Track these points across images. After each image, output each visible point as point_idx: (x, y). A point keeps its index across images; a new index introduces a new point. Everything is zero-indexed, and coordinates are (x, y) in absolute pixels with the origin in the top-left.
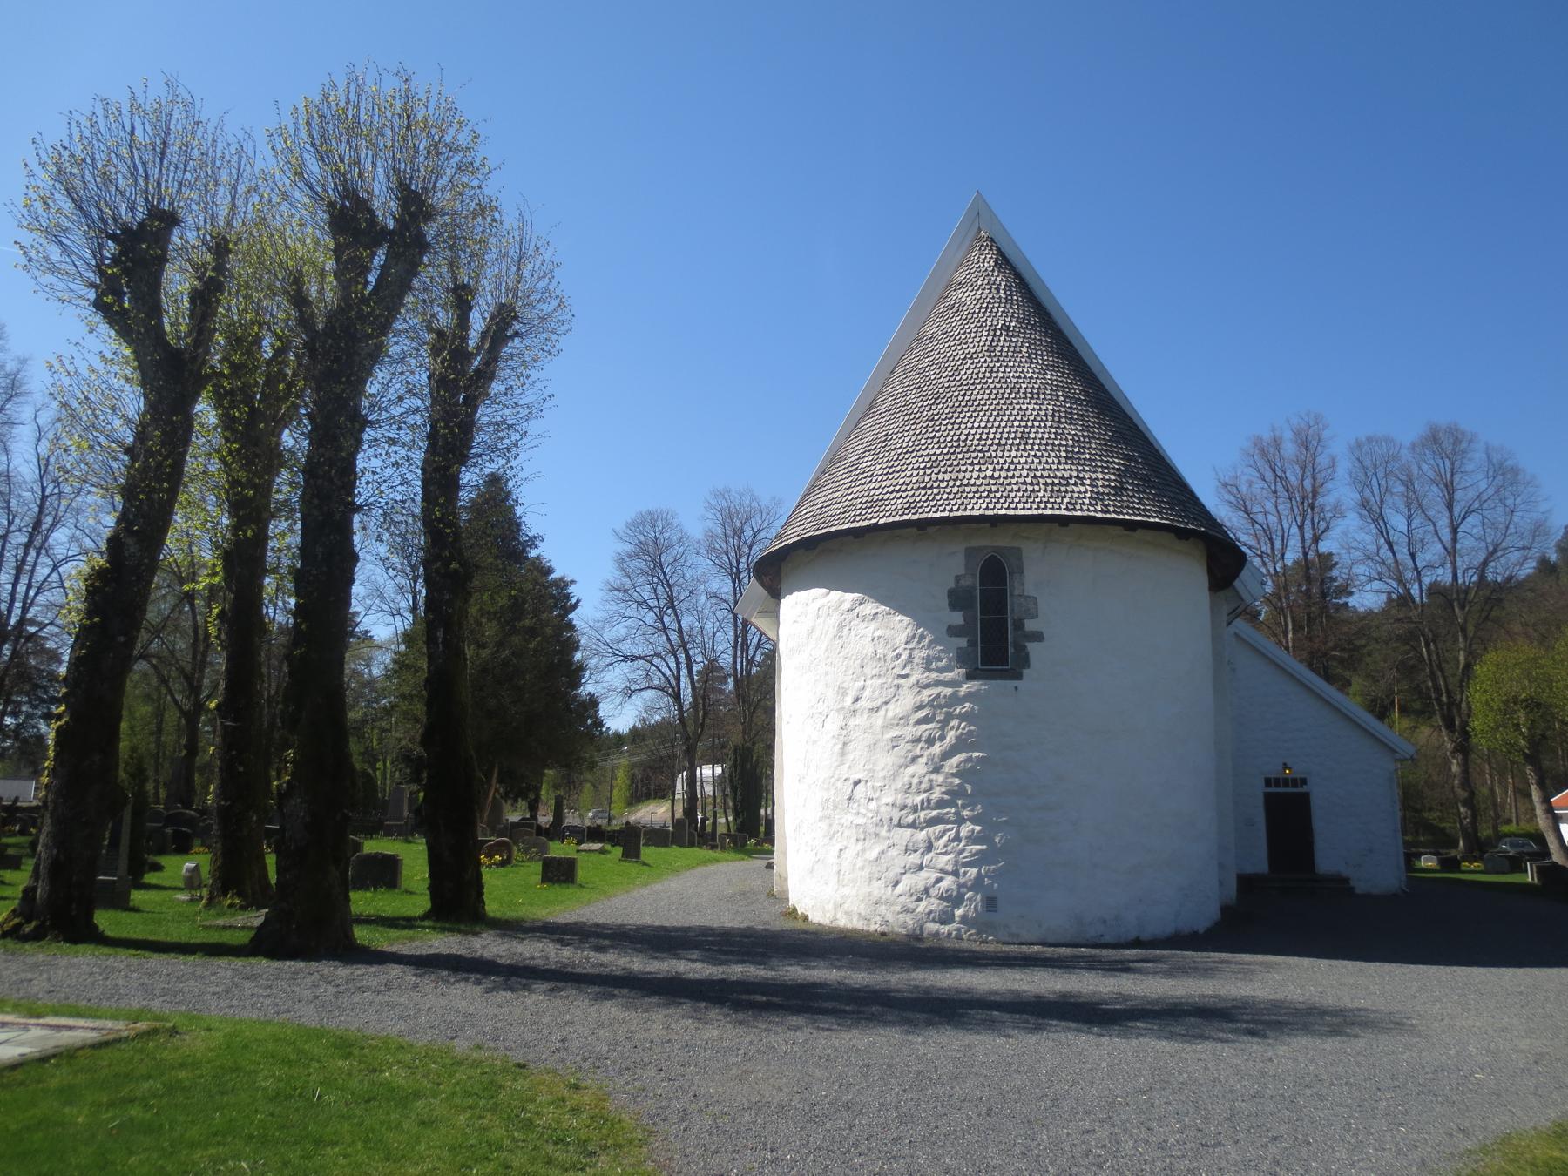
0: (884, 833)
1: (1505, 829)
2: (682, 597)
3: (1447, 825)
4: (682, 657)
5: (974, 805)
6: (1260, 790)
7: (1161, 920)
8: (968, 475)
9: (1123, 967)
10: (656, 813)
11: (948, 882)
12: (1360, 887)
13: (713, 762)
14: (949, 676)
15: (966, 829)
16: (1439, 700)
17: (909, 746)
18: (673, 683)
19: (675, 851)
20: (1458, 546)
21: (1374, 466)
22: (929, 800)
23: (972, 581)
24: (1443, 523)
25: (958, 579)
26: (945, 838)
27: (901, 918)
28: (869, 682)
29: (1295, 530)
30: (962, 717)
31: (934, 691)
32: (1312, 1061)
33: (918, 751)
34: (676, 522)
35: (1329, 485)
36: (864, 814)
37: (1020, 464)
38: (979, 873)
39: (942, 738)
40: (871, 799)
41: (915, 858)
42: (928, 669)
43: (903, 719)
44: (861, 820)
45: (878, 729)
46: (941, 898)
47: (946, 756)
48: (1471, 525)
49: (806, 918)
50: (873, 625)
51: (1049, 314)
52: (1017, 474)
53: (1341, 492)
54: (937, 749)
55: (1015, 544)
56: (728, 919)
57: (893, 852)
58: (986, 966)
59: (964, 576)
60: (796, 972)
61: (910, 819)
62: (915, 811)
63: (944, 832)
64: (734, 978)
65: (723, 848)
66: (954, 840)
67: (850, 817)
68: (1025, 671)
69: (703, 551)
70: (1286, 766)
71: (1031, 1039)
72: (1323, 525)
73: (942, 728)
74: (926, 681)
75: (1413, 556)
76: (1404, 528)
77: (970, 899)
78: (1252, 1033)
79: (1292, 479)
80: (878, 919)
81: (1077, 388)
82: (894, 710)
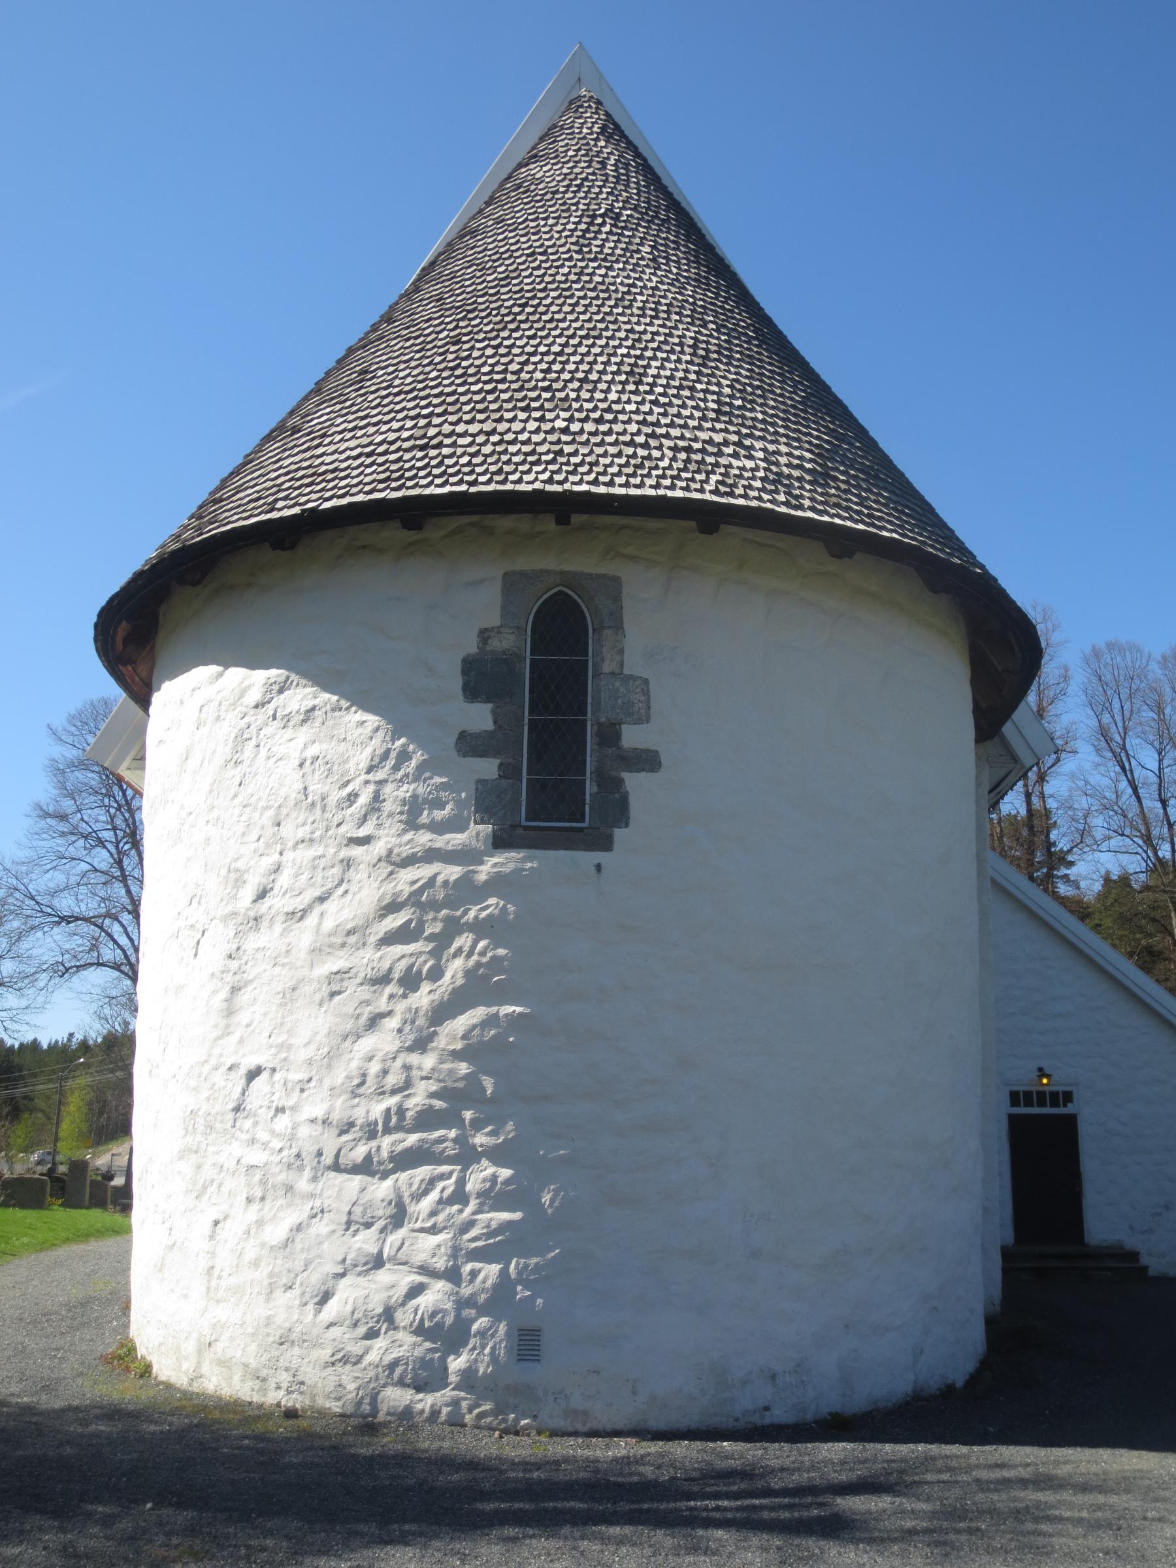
0: (303, 1184)
7: (886, 1378)
11: (436, 1295)
14: (456, 840)
15: (479, 1175)
17: (365, 992)
22: (401, 1111)
23: (515, 642)
25: (484, 635)
26: (434, 1196)
28: (289, 856)
30: (480, 928)
33: (382, 1004)
36: (260, 1145)
39: (436, 974)
40: (280, 1110)
41: (365, 1242)
42: (411, 824)
43: (355, 932)
44: (257, 1157)
45: (301, 953)
47: (442, 1012)
49: (146, 1371)
50: (304, 734)
52: (618, 428)
54: (424, 998)
57: (321, 1227)
59: (498, 630)
61: (361, 1151)
62: (371, 1132)
63: (432, 1182)
67: (237, 1149)
68: (619, 834)
70: (1042, 1073)
73: (436, 953)
74: (406, 851)
76: (1154, 766)
77: (482, 1334)
80: (284, 1378)
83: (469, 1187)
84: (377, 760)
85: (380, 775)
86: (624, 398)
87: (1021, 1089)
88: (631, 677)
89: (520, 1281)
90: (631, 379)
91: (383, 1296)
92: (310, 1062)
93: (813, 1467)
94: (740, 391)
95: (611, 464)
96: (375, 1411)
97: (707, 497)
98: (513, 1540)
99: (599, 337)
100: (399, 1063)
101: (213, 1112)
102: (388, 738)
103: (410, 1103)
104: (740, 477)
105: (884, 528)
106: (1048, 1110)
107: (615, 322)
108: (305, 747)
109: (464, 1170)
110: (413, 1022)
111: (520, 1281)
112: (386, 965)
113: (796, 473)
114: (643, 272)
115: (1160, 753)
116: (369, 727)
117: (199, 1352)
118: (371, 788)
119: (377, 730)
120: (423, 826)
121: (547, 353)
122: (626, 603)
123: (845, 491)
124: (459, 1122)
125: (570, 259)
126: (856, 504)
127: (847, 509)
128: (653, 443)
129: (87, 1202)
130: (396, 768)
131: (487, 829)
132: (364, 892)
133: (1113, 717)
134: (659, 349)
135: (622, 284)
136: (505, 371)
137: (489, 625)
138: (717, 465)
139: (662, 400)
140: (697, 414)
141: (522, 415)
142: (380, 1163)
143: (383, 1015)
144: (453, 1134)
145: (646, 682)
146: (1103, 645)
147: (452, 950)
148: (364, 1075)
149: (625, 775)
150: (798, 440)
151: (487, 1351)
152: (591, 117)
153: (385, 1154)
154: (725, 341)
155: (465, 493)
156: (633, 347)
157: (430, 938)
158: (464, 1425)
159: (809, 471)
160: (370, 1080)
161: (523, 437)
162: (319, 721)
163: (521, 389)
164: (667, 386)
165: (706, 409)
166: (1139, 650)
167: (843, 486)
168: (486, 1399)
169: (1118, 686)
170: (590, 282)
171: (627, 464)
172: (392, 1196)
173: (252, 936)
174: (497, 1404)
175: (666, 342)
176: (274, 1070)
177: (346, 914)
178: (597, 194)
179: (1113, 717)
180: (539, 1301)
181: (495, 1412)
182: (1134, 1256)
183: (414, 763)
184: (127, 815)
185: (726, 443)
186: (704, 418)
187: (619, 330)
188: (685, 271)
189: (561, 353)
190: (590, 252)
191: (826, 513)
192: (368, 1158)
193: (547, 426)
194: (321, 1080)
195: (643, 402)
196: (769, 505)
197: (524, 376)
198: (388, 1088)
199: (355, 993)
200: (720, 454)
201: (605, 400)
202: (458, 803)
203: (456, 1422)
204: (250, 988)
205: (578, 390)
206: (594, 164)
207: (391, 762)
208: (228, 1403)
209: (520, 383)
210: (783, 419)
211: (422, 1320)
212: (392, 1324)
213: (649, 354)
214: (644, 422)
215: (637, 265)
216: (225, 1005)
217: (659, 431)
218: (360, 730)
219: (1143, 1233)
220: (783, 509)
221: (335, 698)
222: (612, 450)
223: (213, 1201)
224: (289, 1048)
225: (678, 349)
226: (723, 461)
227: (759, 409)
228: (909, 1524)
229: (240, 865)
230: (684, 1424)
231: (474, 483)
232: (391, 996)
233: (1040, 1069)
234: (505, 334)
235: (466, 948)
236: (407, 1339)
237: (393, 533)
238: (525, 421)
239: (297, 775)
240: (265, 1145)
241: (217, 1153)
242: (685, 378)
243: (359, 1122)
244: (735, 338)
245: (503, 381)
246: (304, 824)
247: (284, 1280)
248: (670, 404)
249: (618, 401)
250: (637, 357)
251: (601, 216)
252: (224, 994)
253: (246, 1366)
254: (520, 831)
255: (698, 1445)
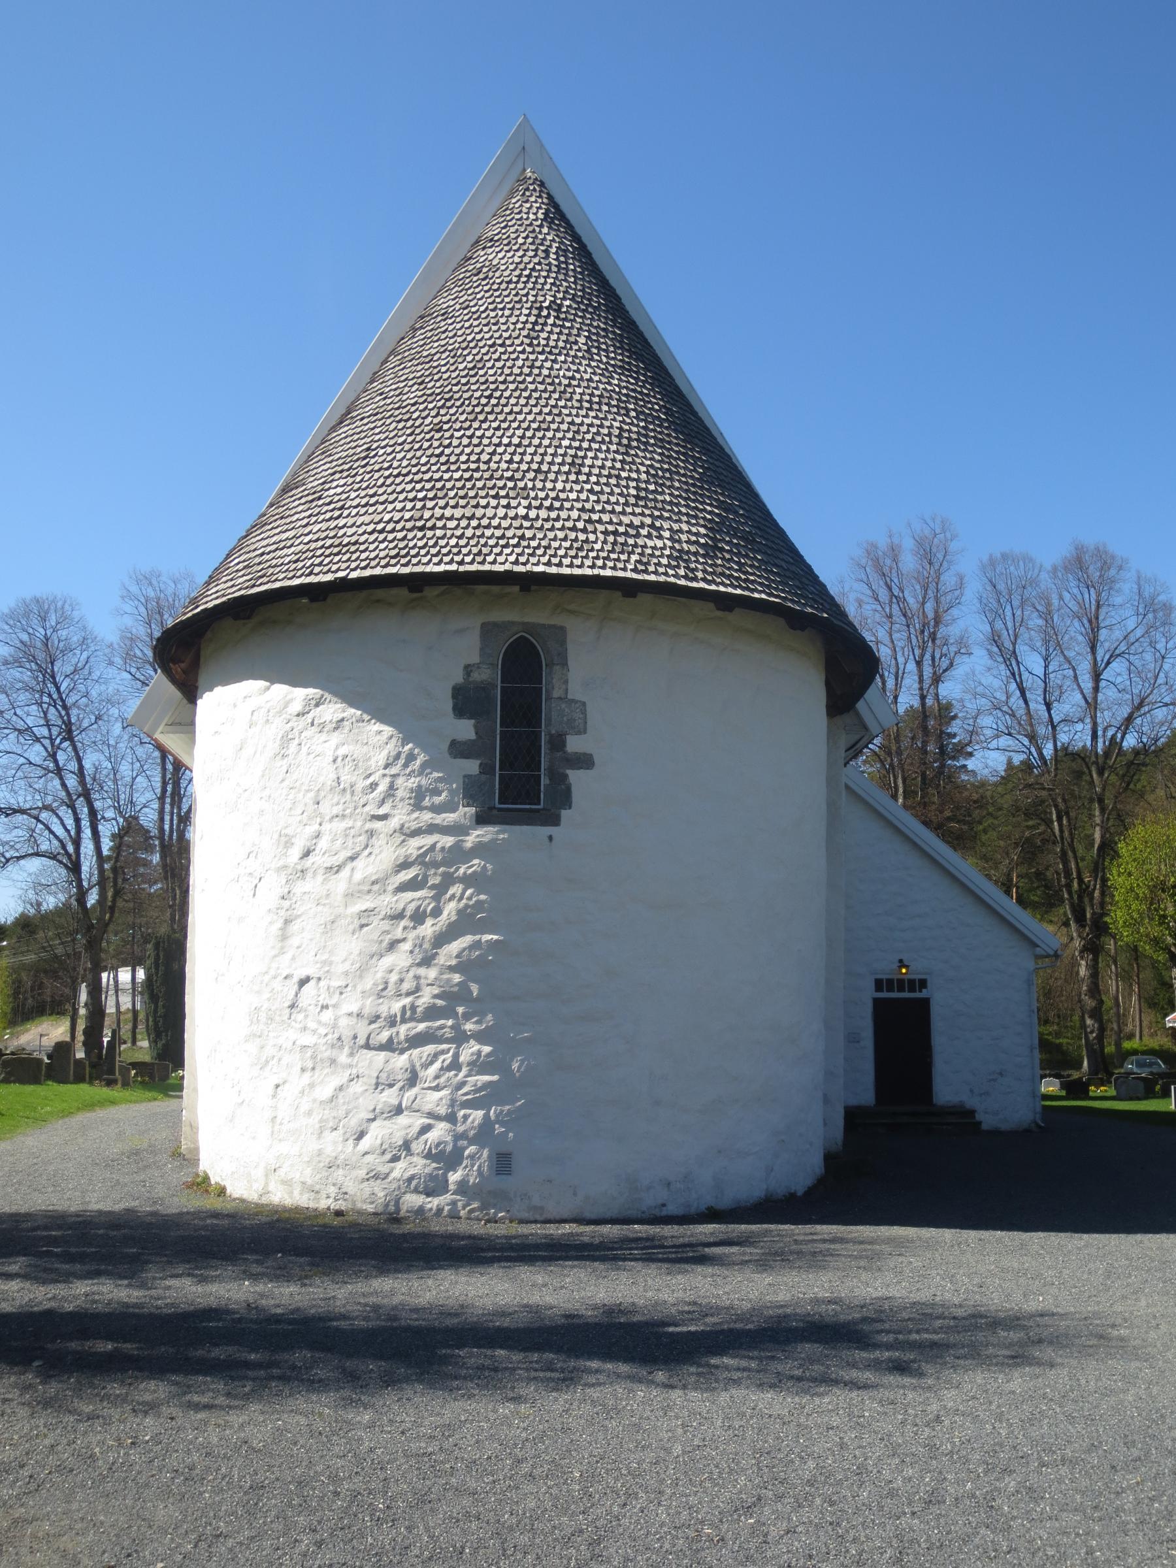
0: (343, 1058)
1: (1127, 1045)
2: (85, 724)
3: (1064, 1041)
4: (84, 812)
5: (482, 1015)
6: (868, 994)
7: (747, 1180)
8: (490, 512)
9: (690, 1256)
10: (45, 1034)
11: (440, 1132)
12: (988, 1121)
13: (134, 962)
14: (450, 818)
15: (469, 1051)
16: (1069, 886)
17: (386, 924)
18: (71, 848)
19: (51, 1090)
20: (1100, 697)
21: (1009, 591)
22: (413, 1008)
24: (1084, 668)
25: (468, 669)
26: (437, 1065)
27: (367, 1188)
28: (327, 827)
29: (911, 666)
30: (467, 881)
31: (427, 841)
32: (1000, 1417)
33: (398, 933)
34: (76, 614)
35: (955, 612)
36: (312, 1029)
37: (563, 501)
38: (486, 1117)
39: (437, 912)
40: (325, 1007)
41: (390, 1097)
42: (418, 806)
43: (377, 884)
44: (308, 1039)
45: (339, 898)
46: (429, 1156)
47: (441, 940)
48: (1116, 671)
49: (222, 1191)
50: (336, 738)
51: (618, 298)
52: (564, 514)
53: (967, 622)
54: (428, 929)
55: (556, 621)
56: (98, 1196)
57: (357, 1088)
58: (490, 1261)
59: (478, 666)
60: (182, 1290)
61: (385, 1035)
62: (392, 1022)
63: (436, 1056)
64: (69, 1307)
65: (126, 1084)
66: (449, 1068)
67: (292, 1034)
68: (565, 813)
69: (118, 660)
70: (902, 964)
71: (557, 1402)
72: (945, 663)
73: (437, 898)
74: (414, 826)
75: (1048, 706)
76: (1040, 671)
77: (472, 1157)
78: (900, 1368)
79: (911, 601)
80: (332, 1190)
81: (656, 403)
82: (365, 869)
83: (462, 1059)
84: (391, 759)
85: (394, 770)
86: (568, 487)
87: (884, 977)
88: (573, 701)
89: (497, 1122)
90: (573, 470)
91: (403, 1133)
92: (346, 974)
93: (692, 1236)
94: (653, 476)
95: (559, 548)
96: (398, 1210)
97: (629, 574)
98: (509, 1267)
99: (548, 429)
100: (411, 974)
101: (273, 1008)
102: (399, 743)
103: (420, 1002)
104: (652, 555)
105: (756, 590)
106: (906, 995)
107: (559, 414)
108: (337, 748)
109: (458, 1048)
110: (421, 946)
111: (497, 1122)
112: (401, 906)
113: (693, 549)
114: (580, 364)
115: (1045, 660)
116: (385, 735)
117: (266, 1176)
118: (388, 779)
119: (391, 737)
120: (426, 808)
121: (509, 445)
122: (570, 646)
123: (728, 561)
124: (455, 1015)
125: (523, 352)
126: (736, 571)
127: (729, 577)
128: (590, 528)
129: (71, 1078)
130: (406, 766)
131: (472, 810)
132: (383, 855)
133: (1005, 624)
134: (592, 440)
135: (564, 376)
136: (478, 461)
137: (472, 662)
138: (635, 545)
139: (597, 488)
140: (622, 500)
141: (493, 502)
142: (399, 1043)
143: (399, 941)
144: (450, 1023)
145: (584, 704)
146: (999, 555)
147: (448, 896)
148: (386, 983)
149: (569, 772)
150: (696, 517)
151: (475, 1168)
152: (536, 202)
153: (402, 1037)
154: (643, 427)
155: (456, 572)
156: (573, 439)
157: (433, 887)
158: (460, 1218)
159: (703, 546)
160: (391, 986)
161: (495, 522)
162: (347, 728)
163: (491, 478)
164: (599, 475)
165: (628, 495)
166: (1031, 560)
167: (728, 556)
168: (474, 1200)
169: (1010, 595)
170: (539, 375)
171: (571, 548)
172: (408, 1066)
173: (299, 883)
174: (482, 1204)
175: (598, 433)
176: (319, 979)
177: (371, 870)
178: (543, 284)
179: (1005, 624)
180: (511, 1135)
181: (481, 1209)
182: (972, 1113)
183: (418, 762)
184: (63, 713)
185: (642, 525)
186: (626, 504)
187: (562, 422)
188: (613, 359)
189: (519, 445)
190: (538, 345)
191: (713, 582)
192: (390, 1040)
193: (512, 513)
194: (355, 986)
195: (581, 491)
196: (672, 580)
197: (493, 466)
198: (404, 991)
199: (378, 925)
200: (638, 535)
201: (553, 489)
202: (451, 791)
203: (454, 1216)
204: (299, 920)
205: (534, 480)
206: (540, 253)
207: (402, 761)
208: (291, 1209)
209: (490, 472)
210: (685, 499)
211: (430, 1148)
212: (409, 1152)
213: (585, 445)
214: (582, 510)
215: (575, 356)
216: (280, 933)
217: (595, 517)
218: (378, 737)
219: (981, 1095)
220: (683, 582)
221: (359, 712)
222: (561, 535)
223: (274, 1070)
224: (331, 963)
225: (607, 439)
226: (640, 542)
227: (667, 491)
228: (747, 1258)
229: (289, 831)
230: (608, 1215)
231: (461, 563)
232: (405, 928)
233: (901, 961)
234: (476, 425)
235: (458, 895)
236: (421, 1162)
237: (403, 592)
238: (496, 508)
239: (332, 768)
240: (314, 1031)
241: (277, 1037)
242: (613, 468)
243: (383, 1015)
244: (651, 423)
245: (477, 470)
246: (338, 804)
247: (331, 1124)
248: (602, 492)
249: (563, 491)
250: (577, 448)
251: (547, 308)
252: (280, 924)
253: (303, 1183)
254: (495, 812)
255: (618, 1227)
